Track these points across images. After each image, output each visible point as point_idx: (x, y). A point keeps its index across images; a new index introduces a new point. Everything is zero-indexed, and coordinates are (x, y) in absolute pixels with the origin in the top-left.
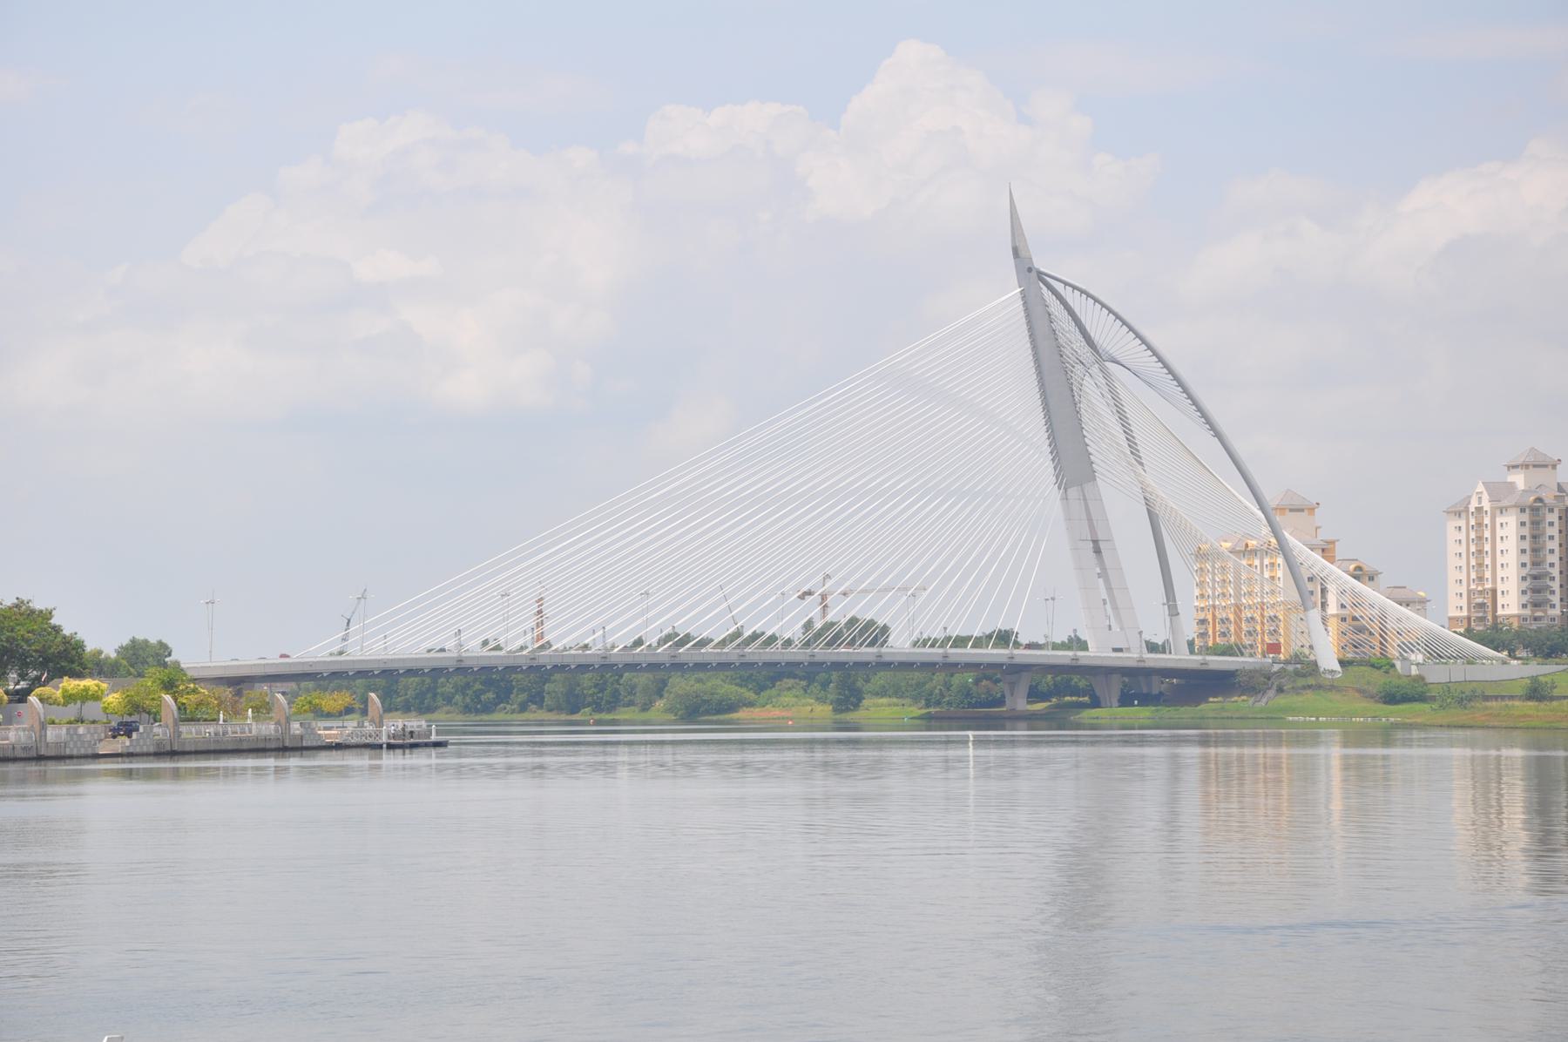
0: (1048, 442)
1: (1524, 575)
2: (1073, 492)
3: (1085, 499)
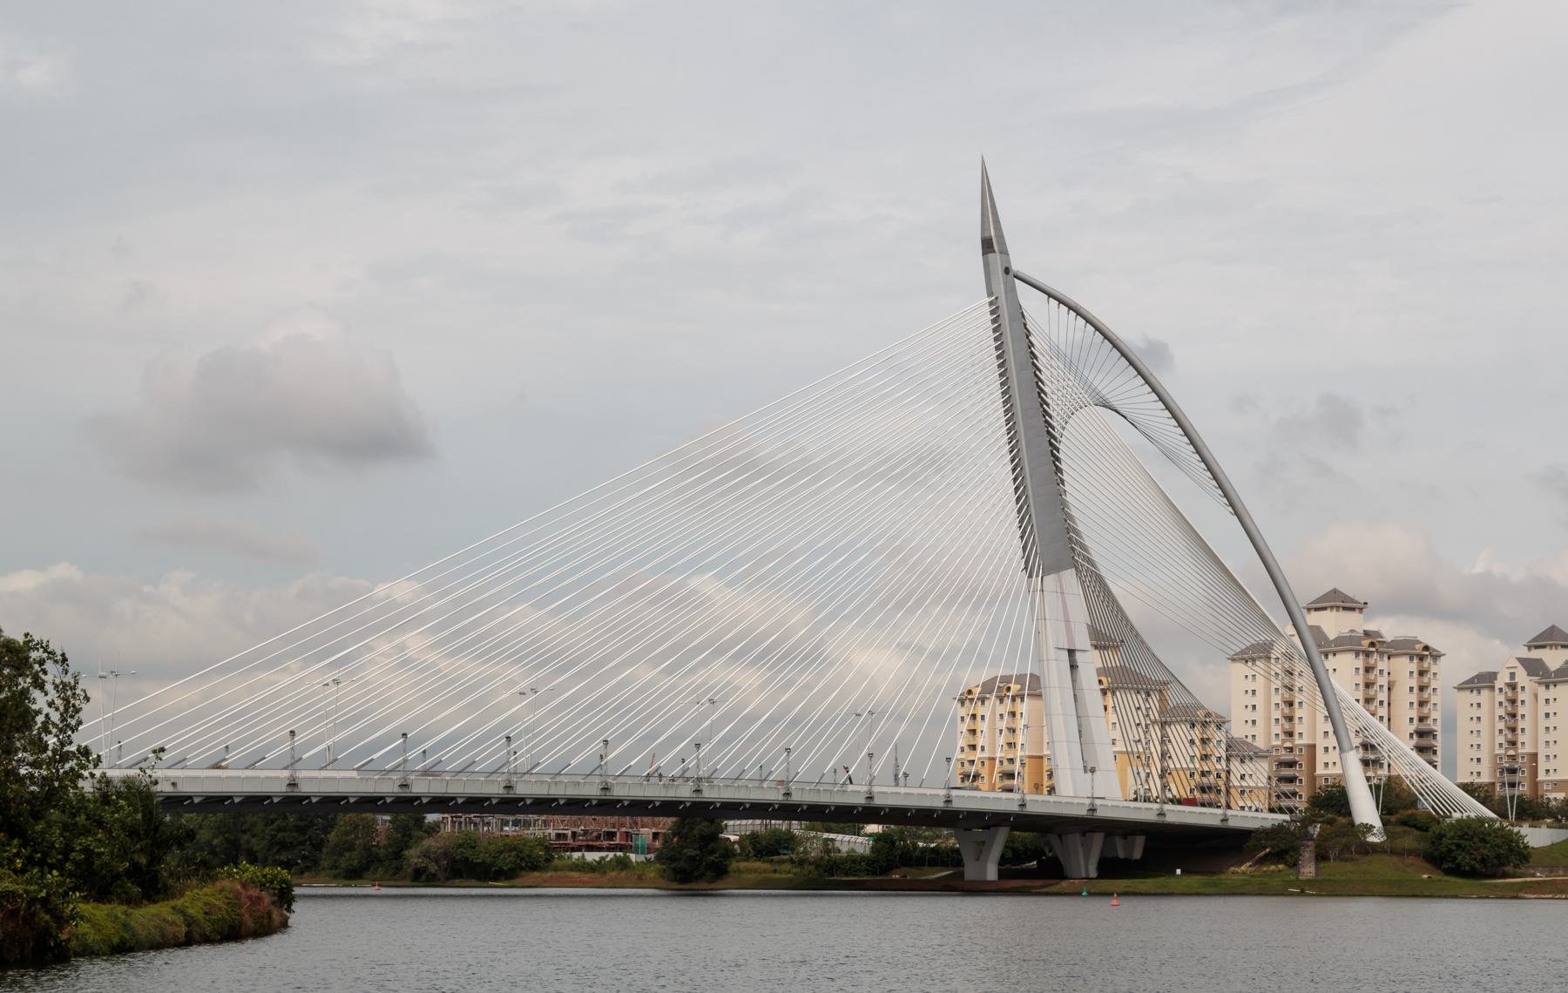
3: (1062, 593)
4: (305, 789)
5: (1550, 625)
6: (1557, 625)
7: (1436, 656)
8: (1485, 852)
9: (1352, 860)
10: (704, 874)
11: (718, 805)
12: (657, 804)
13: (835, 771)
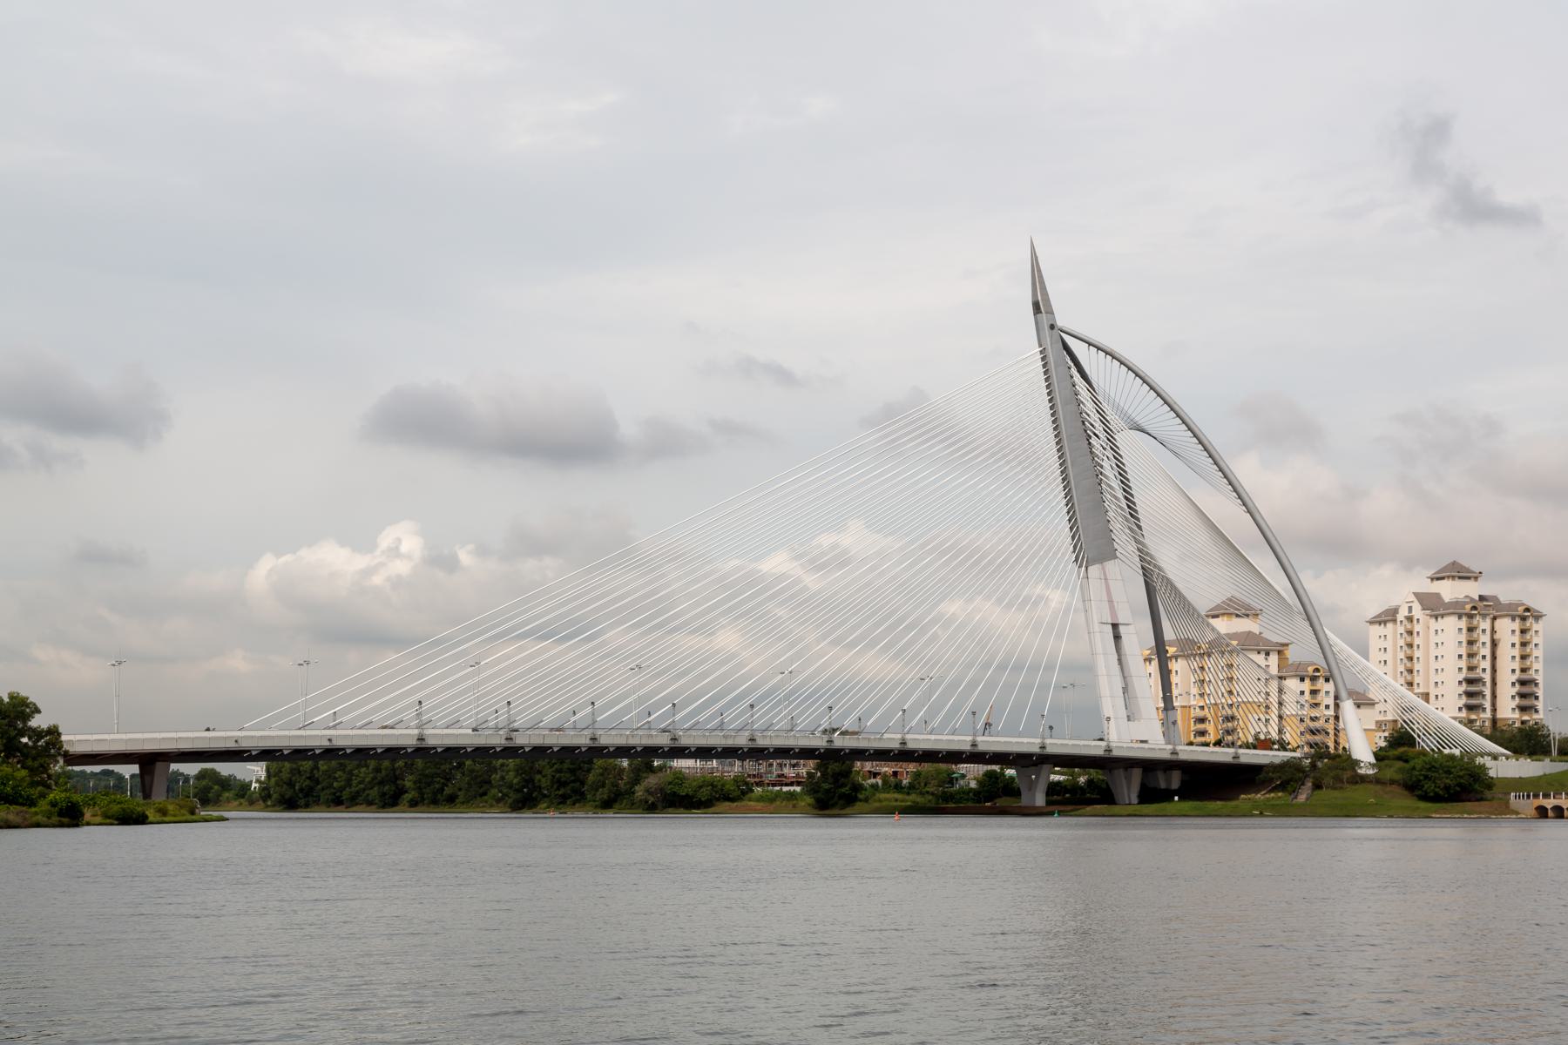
0: (1066, 510)
2: (1094, 570)
3: (1106, 579)
4: (431, 742)
7: (1538, 617)
8: (1448, 781)
9: (1341, 788)
10: (836, 803)
11: (771, 750)
12: (719, 750)
13: (860, 719)
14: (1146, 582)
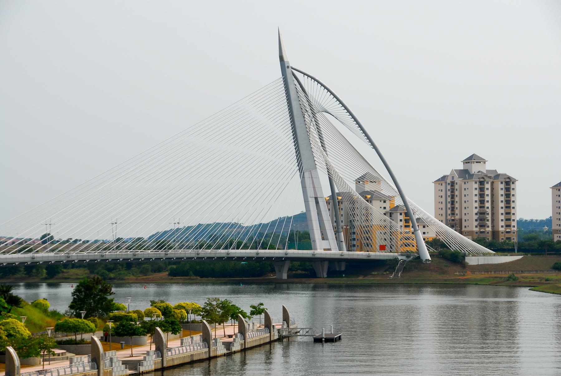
1: (476, 212)
3: (312, 178)
5: (467, 169)
6: (469, 170)
14: (329, 178)
